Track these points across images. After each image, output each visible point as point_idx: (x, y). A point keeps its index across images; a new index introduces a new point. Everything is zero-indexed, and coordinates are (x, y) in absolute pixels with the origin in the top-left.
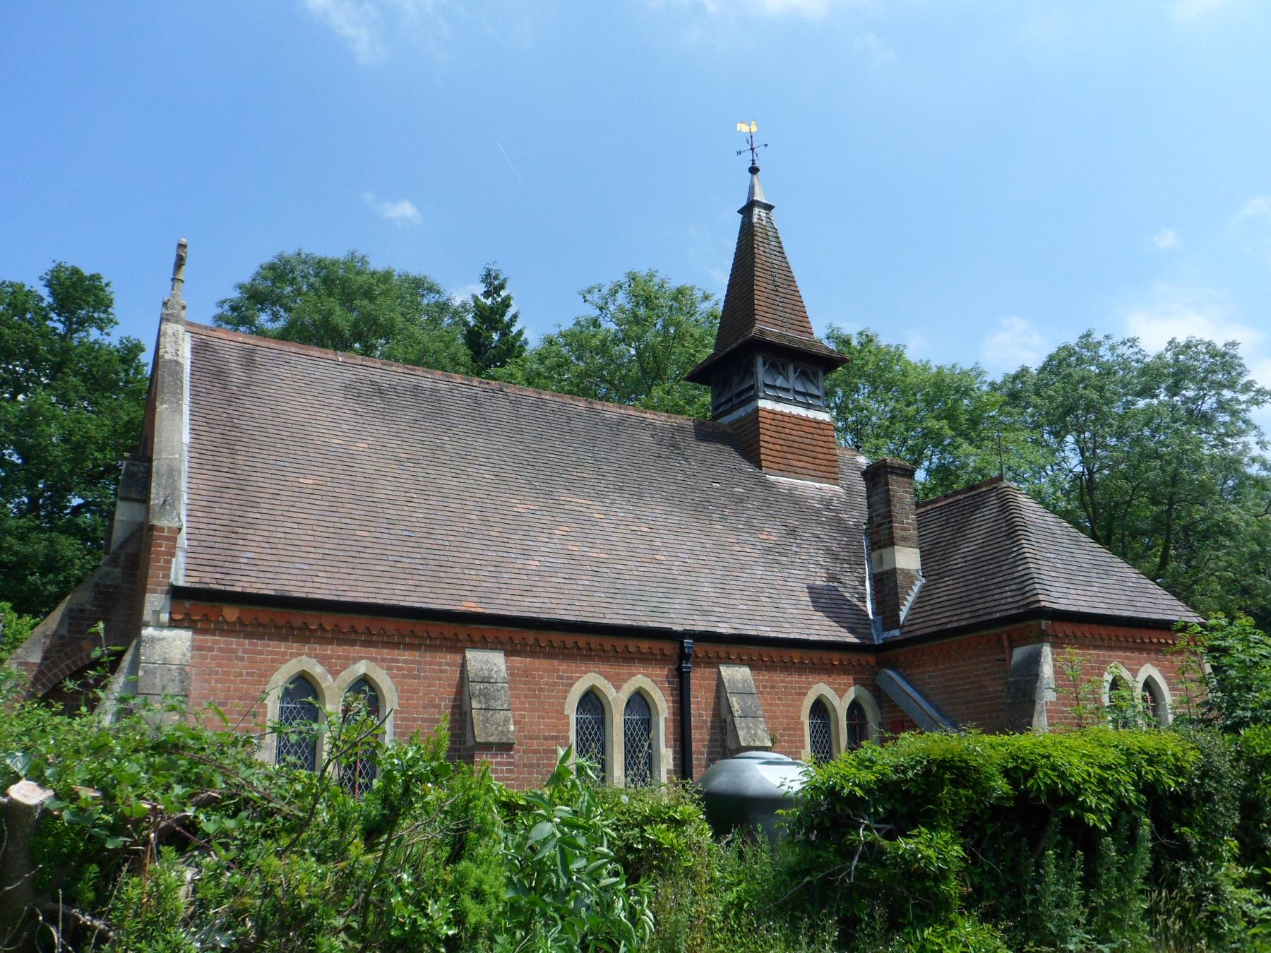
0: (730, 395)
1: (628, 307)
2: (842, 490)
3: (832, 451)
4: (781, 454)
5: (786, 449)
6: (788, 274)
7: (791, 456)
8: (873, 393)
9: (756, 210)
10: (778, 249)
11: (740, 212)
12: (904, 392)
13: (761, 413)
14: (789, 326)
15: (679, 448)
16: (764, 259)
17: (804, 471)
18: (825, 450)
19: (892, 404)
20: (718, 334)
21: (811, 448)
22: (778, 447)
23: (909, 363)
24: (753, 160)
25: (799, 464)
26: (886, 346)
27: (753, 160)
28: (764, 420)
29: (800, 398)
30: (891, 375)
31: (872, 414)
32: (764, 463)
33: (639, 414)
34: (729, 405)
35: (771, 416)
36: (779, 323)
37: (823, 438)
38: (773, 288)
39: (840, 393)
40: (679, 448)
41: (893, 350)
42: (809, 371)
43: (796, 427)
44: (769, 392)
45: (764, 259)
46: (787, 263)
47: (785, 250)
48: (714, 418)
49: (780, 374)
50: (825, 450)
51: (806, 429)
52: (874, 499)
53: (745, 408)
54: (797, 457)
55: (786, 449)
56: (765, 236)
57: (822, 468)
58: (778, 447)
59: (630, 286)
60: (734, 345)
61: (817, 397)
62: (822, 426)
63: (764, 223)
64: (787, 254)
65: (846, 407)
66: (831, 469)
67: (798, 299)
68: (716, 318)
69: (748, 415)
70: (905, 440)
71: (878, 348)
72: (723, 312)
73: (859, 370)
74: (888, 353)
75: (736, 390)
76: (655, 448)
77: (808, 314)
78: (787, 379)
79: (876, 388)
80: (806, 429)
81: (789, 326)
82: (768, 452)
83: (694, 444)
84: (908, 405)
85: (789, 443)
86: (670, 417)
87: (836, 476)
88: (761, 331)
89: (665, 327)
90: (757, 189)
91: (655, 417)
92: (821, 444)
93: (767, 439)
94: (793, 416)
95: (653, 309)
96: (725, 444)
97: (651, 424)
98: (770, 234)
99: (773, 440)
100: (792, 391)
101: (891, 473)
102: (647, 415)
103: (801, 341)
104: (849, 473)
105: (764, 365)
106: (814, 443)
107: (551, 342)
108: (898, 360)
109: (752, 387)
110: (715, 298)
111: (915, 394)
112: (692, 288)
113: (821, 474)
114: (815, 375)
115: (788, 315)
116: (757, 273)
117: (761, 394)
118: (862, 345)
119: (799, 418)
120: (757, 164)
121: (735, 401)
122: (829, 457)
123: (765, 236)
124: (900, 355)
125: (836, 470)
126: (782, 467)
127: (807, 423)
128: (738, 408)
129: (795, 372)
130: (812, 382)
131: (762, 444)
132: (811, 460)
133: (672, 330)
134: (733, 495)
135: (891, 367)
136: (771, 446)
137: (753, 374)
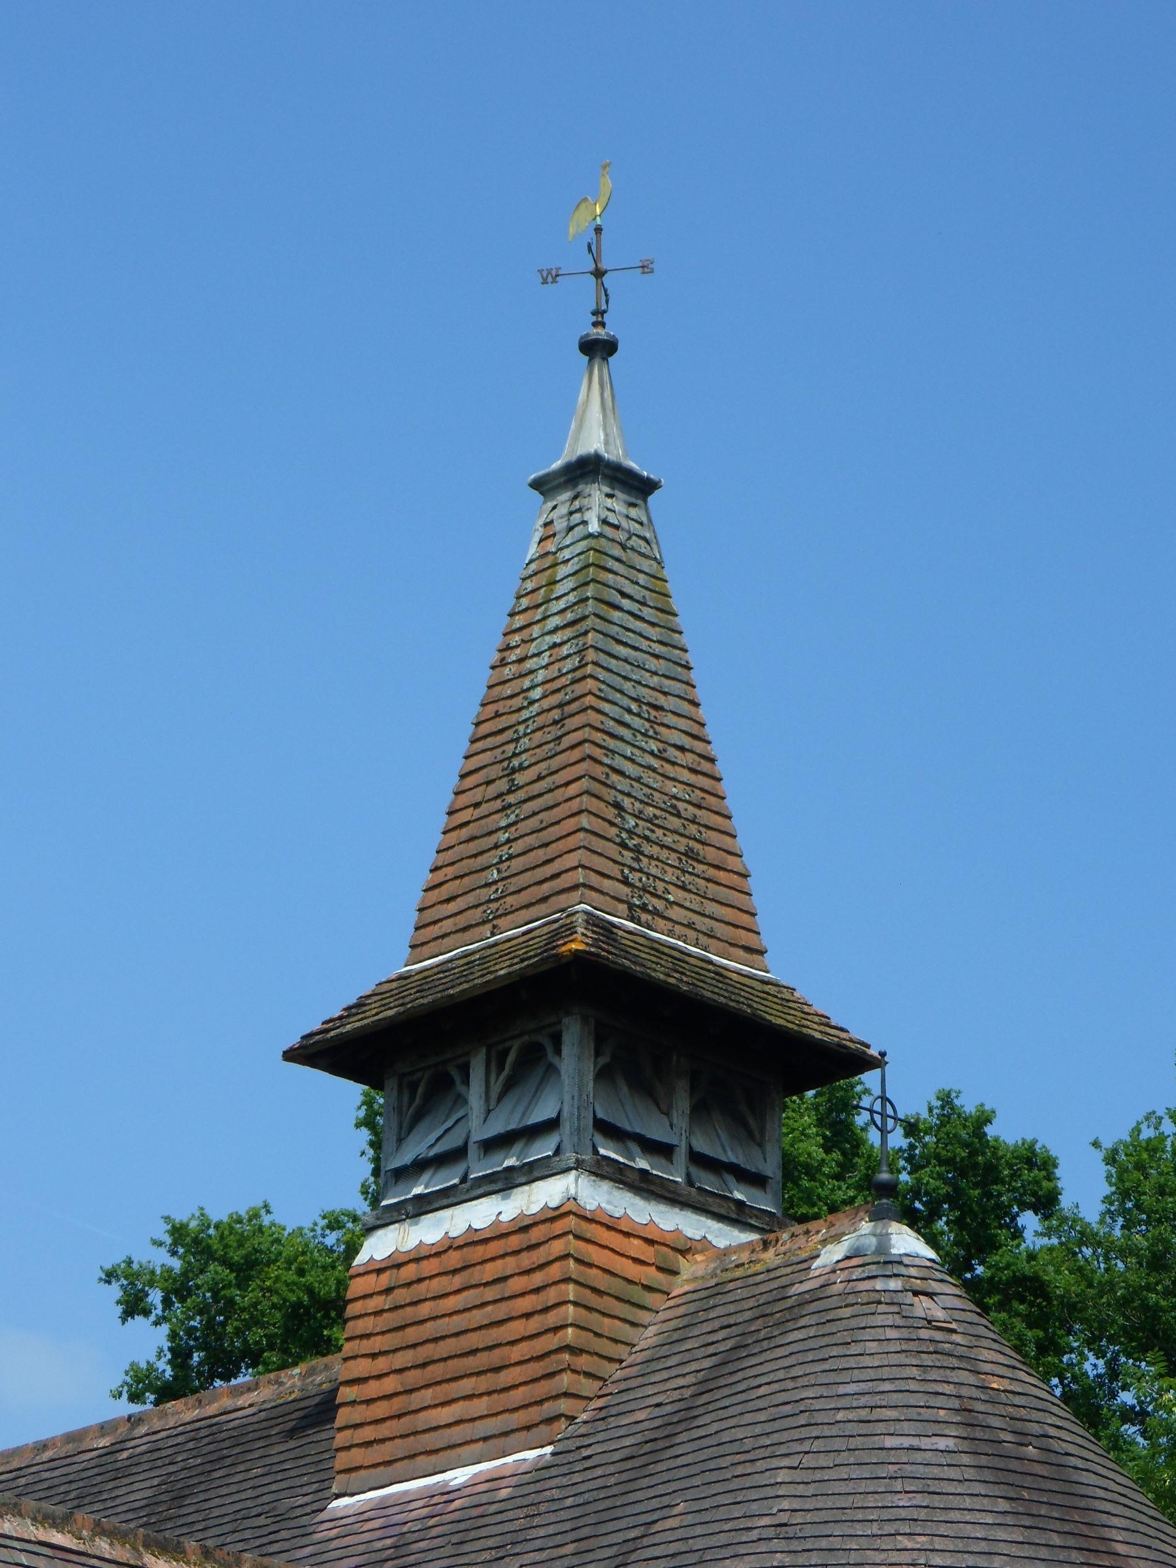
119: (498, 1233)
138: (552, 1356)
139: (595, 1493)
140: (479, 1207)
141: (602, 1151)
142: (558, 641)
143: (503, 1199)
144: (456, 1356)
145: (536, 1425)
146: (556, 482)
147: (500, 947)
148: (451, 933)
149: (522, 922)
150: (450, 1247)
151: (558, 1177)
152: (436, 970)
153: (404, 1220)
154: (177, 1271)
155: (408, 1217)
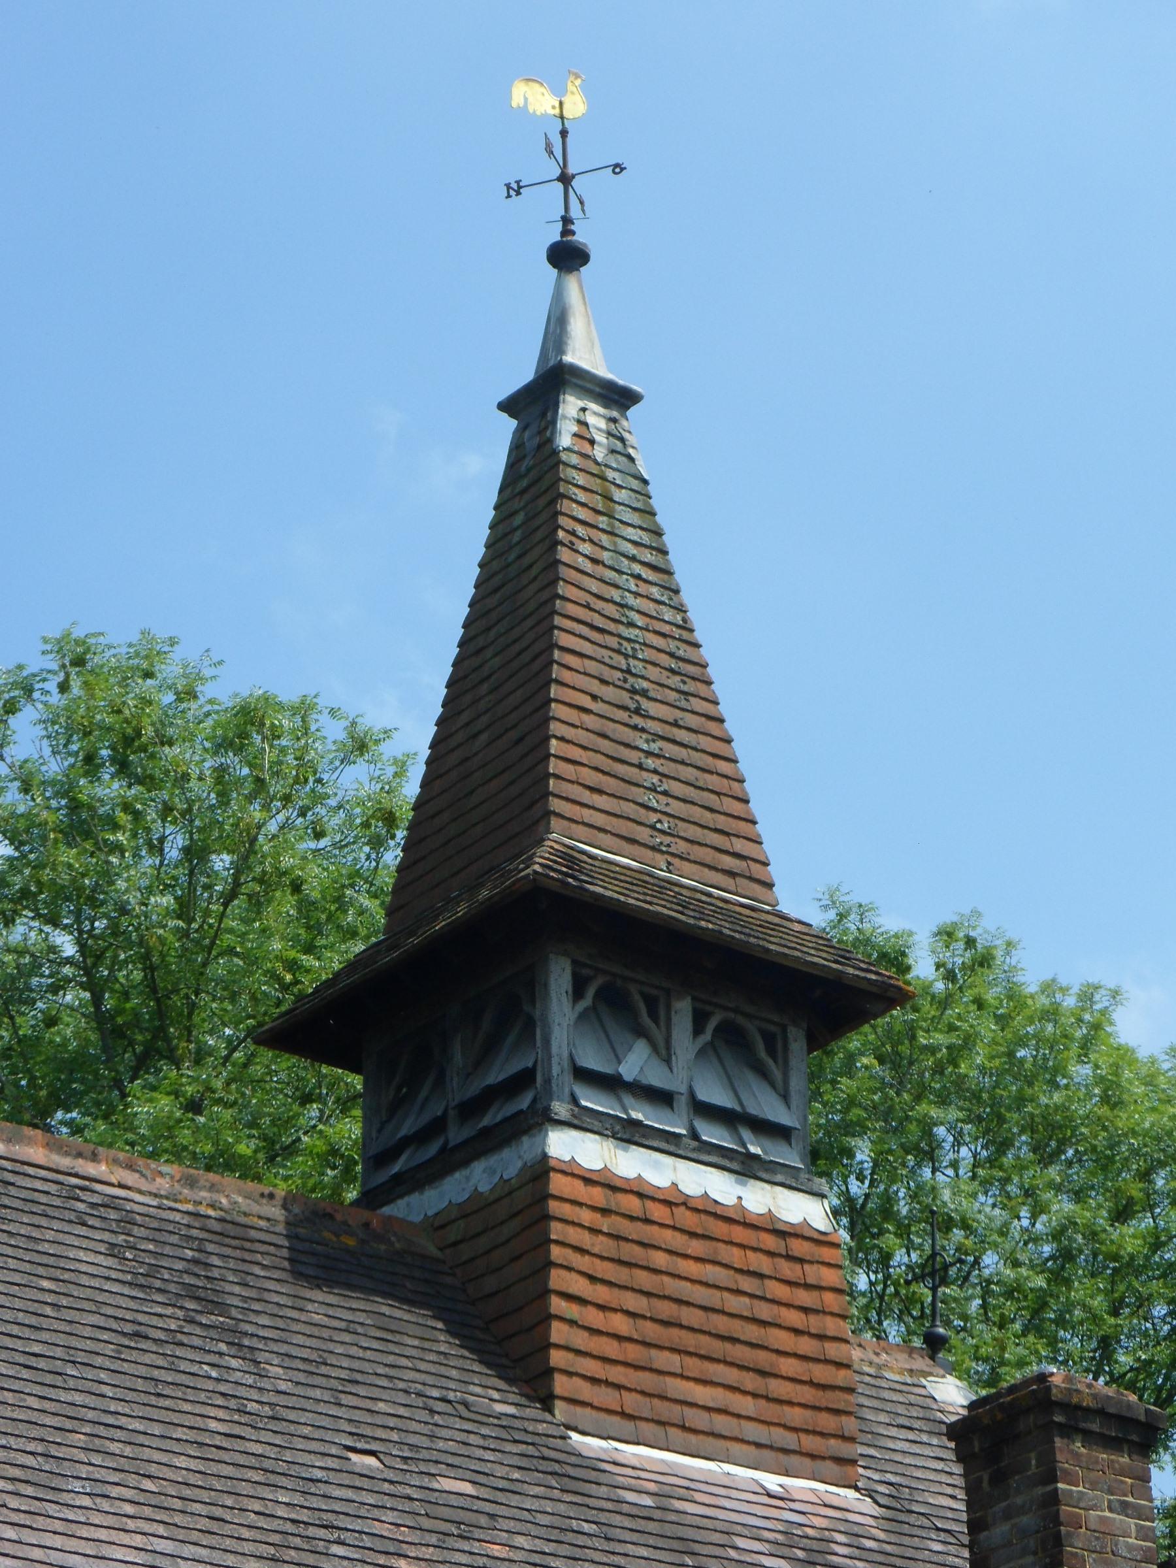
0: (436, 1109)
1: (54, 768)
2: (868, 1506)
3: (833, 1350)
4: (633, 1352)
5: (651, 1331)
6: (683, 651)
7: (671, 1361)
8: (992, 1162)
9: (571, 405)
10: (648, 556)
11: (509, 406)
12: (1105, 1163)
13: (558, 1184)
14: (681, 847)
15: (221, 1308)
16: (594, 586)
17: (721, 1423)
18: (806, 1345)
19: (1063, 1206)
20: (398, 888)
21: (752, 1332)
22: (620, 1324)
23: (1125, 1055)
24: (566, 220)
25: (701, 1394)
26: (1049, 987)
27: (566, 220)
28: (566, 1210)
29: (712, 1134)
30: (1057, 1097)
31: (984, 1244)
32: (561, 1385)
33: (65, 1162)
34: (433, 1149)
35: (597, 1195)
36: (643, 834)
37: (804, 1297)
38: (624, 698)
39: (863, 1153)
40: (221, 1308)
41: (1070, 1002)
42: (751, 1028)
43: (696, 1247)
44: (592, 1101)
45: (594, 586)
46: (681, 609)
47: (675, 559)
48: (371, 1199)
49: (640, 1032)
50: (806, 1345)
51: (735, 1256)
52: (999, 1532)
53: (493, 1160)
54: (694, 1366)
55: (651, 1331)
56: (598, 502)
57: (795, 1415)
58: (620, 1324)
59: (64, 687)
60: (461, 910)
61: (780, 1132)
62: (798, 1247)
63: (599, 453)
64: (681, 577)
65: (887, 1210)
66: (827, 1422)
67: (718, 748)
68: (390, 819)
69: (506, 1191)
70: (1106, 1345)
71: (1014, 995)
72: (418, 806)
73: (939, 1070)
74: (1051, 1014)
75: (460, 1090)
76: (120, 1297)
77: (756, 807)
78: (664, 1054)
79: (1004, 1146)
80: (735, 1256)
81: (681, 847)
82: (580, 1339)
83: (281, 1291)
84: (1122, 1214)
85: (666, 1309)
86: (191, 1182)
87: (846, 1450)
88: (570, 858)
89: (195, 854)
90: (578, 326)
91: (130, 1178)
92: (794, 1318)
93: (579, 1285)
94: (685, 1202)
95: (148, 781)
96: (410, 1301)
97: (111, 1203)
98: (620, 495)
99: (601, 1293)
100: (682, 1102)
101: (1069, 1431)
102: (99, 1170)
103: (724, 910)
104: (899, 1441)
105: (578, 993)
106: (764, 1311)
107: (47, 1144)
108: (1086, 1045)
109: (525, 1079)
110: (389, 749)
111: (1145, 1176)
112: (304, 710)
113: (789, 1440)
114: (775, 1045)
115: (676, 807)
116: (564, 640)
117: (561, 1109)
118: (950, 976)
119: (707, 1209)
120: (582, 235)
121: (456, 1134)
122: (821, 1373)
123: (598, 502)
124: (1097, 1027)
125: (850, 1425)
126: (631, 1402)
127: (739, 1234)
128: (466, 1163)
129: (698, 1030)
130: (763, 1073)
131: (557, 1305)
132: (750, 1381)
133: (221, 862)
134: (433, 1501)
135: (1060, 1069)
136: (593, 1317)
137: (530, 1025)
138: (837, 1392)
139: (30, 1303)
140: (709, 1175)
141: (584, 1103)
142: (644, 576)
143: (737, 1182)
144: (709, 1334)
145: (823, 1458)
146: (589, 385)
147: (730, 907)
148: (610, 832)
149: (710, 883)
150: (684, 1204)
151: (807, 1196)
152: (656, 881)
153: (607, 1136)
154: (65, 955)
155: (613, 1137)
